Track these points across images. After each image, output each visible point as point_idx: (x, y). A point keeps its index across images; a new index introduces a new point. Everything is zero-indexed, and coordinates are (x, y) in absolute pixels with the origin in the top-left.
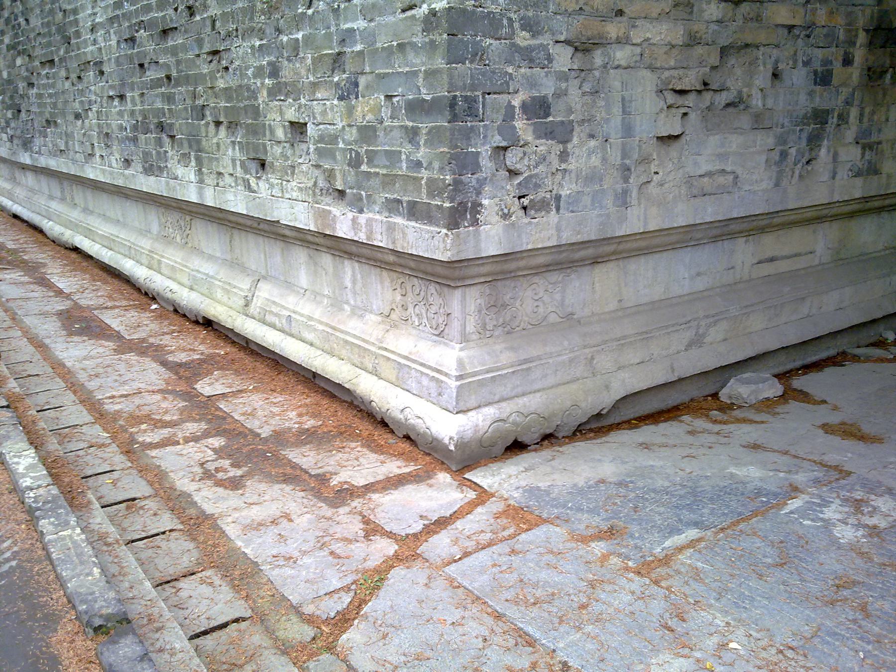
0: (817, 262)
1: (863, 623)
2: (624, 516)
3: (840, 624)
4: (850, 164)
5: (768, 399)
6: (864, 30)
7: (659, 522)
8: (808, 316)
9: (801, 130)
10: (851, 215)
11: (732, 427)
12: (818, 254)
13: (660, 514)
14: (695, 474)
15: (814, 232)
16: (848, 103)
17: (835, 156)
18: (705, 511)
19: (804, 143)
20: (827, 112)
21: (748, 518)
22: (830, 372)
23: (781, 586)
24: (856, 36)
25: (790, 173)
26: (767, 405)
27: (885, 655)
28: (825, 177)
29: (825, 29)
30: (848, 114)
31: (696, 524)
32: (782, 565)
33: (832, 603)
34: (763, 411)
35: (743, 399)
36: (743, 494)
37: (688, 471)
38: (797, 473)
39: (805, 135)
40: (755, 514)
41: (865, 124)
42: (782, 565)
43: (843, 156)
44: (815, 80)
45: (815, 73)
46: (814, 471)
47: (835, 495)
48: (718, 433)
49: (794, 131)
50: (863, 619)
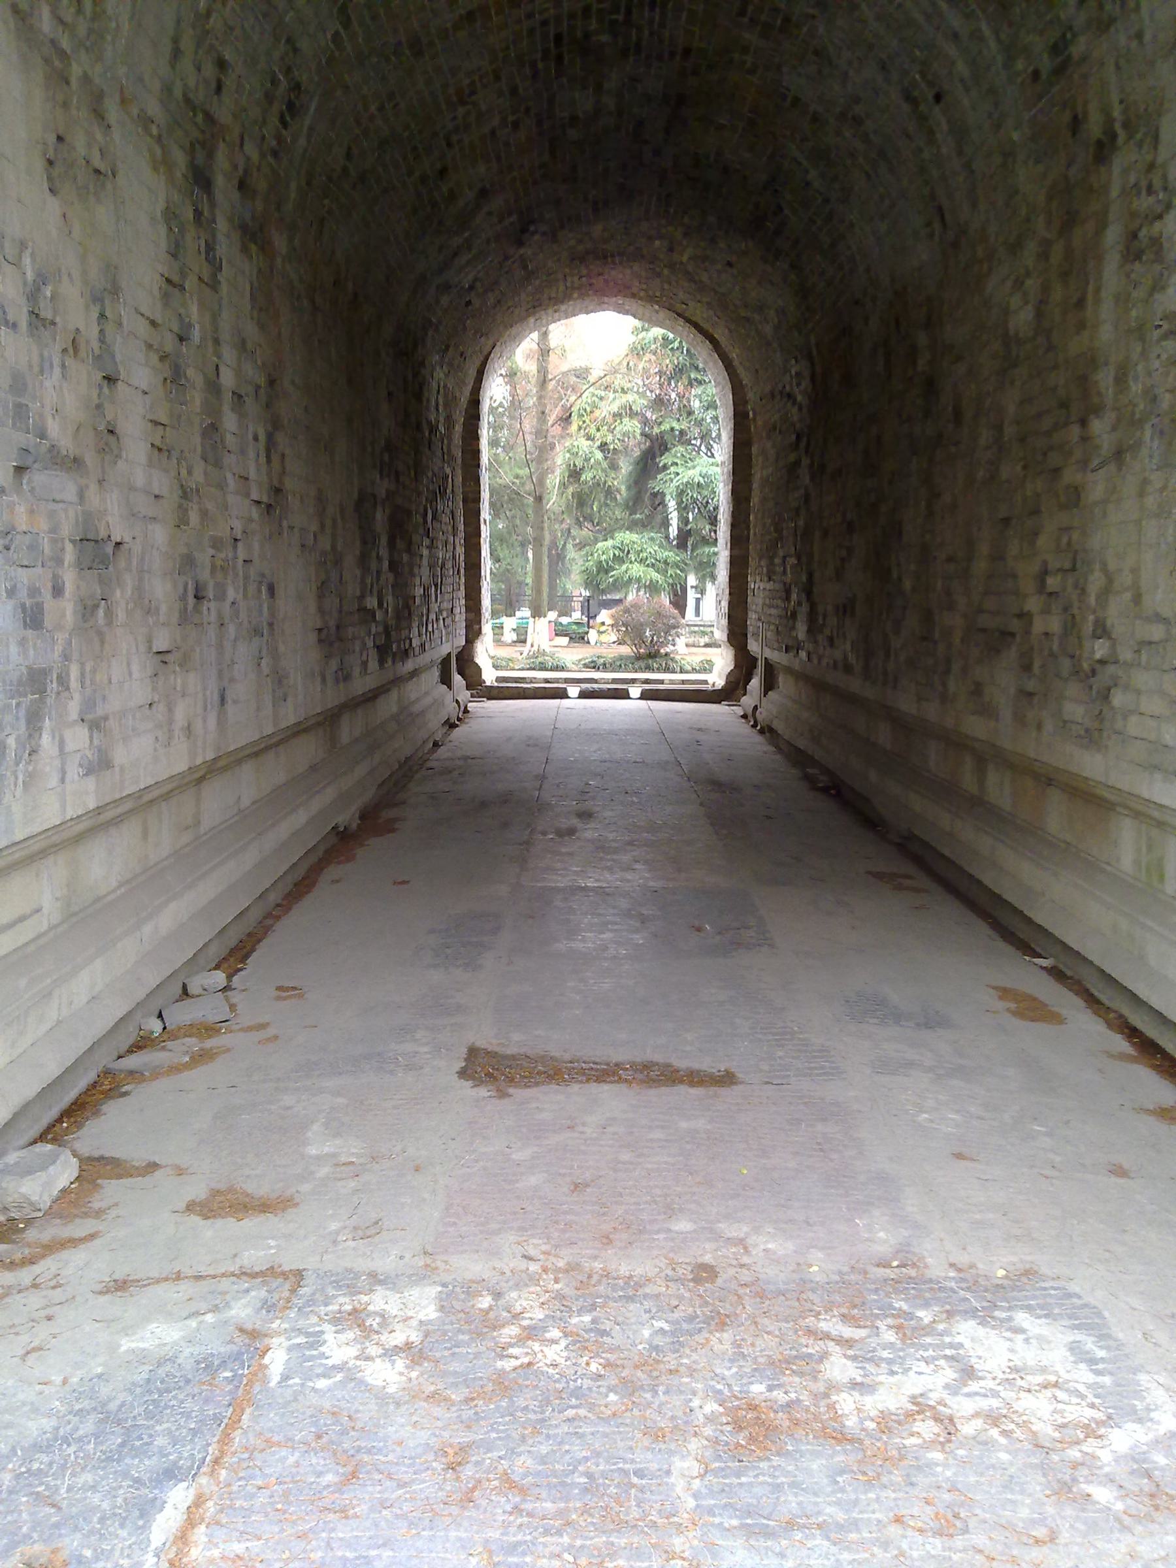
0: (45, 927)
1: (528, 1506)
2: (33, 1529)
3: (506, 1525)
4: (79, 755)
5: (64, 1191)
6: (71, 541)
7: (105, 1505)
8: (59, 1022)
9: (18, 705)
10: (78, 839)
11: (46, 1267)
12: (45, 911)
13: (94, 1488)
14: (75, 1380)
15: (37, 875)
16: (66, 657)
17: (62, 743)
18: (160, 1441)
19: (23, 723)
20: (44, 672)
21: (235, 1422)
22: (113, 1109)
23: (384, 1512)
24: (63, 549)
25: (13, 779)
26: (71, 1202)
27: (591, 1539)
28: (54, 781)
29: (28, 536)
30: (68, 675)
31: (171, 1474)
32: (354, 1475)
33: (468, 1499)
34: (76, 1216)
35: (31, 1204)
36: (188, 1381)
37: (58, 1379)
38: (228, 1305)
39: (22, 713)
40: (238, 1407)
41: (88, 691)
42: (354, 1475)
43: (70, 746)
44: (25, 622)
45: (23, 606)
46: (247, 1291)
47: (315, 1319)
48: (35, 1286)
49: (9, 706)
50: (524, 1500)
